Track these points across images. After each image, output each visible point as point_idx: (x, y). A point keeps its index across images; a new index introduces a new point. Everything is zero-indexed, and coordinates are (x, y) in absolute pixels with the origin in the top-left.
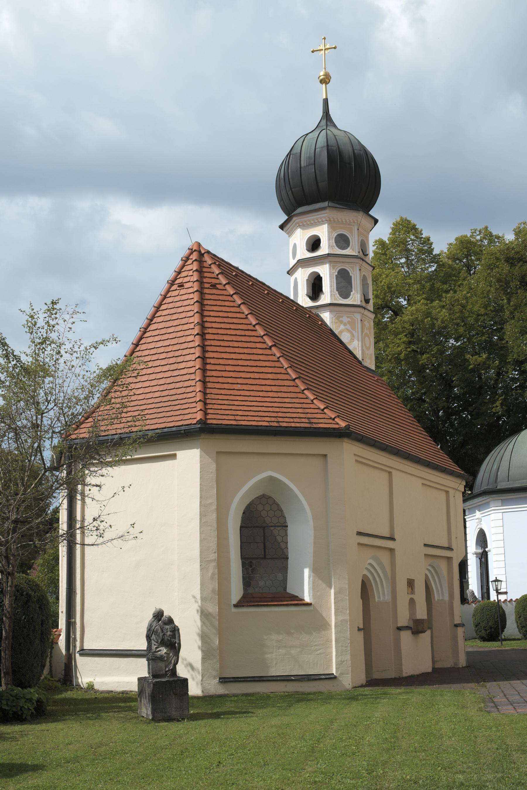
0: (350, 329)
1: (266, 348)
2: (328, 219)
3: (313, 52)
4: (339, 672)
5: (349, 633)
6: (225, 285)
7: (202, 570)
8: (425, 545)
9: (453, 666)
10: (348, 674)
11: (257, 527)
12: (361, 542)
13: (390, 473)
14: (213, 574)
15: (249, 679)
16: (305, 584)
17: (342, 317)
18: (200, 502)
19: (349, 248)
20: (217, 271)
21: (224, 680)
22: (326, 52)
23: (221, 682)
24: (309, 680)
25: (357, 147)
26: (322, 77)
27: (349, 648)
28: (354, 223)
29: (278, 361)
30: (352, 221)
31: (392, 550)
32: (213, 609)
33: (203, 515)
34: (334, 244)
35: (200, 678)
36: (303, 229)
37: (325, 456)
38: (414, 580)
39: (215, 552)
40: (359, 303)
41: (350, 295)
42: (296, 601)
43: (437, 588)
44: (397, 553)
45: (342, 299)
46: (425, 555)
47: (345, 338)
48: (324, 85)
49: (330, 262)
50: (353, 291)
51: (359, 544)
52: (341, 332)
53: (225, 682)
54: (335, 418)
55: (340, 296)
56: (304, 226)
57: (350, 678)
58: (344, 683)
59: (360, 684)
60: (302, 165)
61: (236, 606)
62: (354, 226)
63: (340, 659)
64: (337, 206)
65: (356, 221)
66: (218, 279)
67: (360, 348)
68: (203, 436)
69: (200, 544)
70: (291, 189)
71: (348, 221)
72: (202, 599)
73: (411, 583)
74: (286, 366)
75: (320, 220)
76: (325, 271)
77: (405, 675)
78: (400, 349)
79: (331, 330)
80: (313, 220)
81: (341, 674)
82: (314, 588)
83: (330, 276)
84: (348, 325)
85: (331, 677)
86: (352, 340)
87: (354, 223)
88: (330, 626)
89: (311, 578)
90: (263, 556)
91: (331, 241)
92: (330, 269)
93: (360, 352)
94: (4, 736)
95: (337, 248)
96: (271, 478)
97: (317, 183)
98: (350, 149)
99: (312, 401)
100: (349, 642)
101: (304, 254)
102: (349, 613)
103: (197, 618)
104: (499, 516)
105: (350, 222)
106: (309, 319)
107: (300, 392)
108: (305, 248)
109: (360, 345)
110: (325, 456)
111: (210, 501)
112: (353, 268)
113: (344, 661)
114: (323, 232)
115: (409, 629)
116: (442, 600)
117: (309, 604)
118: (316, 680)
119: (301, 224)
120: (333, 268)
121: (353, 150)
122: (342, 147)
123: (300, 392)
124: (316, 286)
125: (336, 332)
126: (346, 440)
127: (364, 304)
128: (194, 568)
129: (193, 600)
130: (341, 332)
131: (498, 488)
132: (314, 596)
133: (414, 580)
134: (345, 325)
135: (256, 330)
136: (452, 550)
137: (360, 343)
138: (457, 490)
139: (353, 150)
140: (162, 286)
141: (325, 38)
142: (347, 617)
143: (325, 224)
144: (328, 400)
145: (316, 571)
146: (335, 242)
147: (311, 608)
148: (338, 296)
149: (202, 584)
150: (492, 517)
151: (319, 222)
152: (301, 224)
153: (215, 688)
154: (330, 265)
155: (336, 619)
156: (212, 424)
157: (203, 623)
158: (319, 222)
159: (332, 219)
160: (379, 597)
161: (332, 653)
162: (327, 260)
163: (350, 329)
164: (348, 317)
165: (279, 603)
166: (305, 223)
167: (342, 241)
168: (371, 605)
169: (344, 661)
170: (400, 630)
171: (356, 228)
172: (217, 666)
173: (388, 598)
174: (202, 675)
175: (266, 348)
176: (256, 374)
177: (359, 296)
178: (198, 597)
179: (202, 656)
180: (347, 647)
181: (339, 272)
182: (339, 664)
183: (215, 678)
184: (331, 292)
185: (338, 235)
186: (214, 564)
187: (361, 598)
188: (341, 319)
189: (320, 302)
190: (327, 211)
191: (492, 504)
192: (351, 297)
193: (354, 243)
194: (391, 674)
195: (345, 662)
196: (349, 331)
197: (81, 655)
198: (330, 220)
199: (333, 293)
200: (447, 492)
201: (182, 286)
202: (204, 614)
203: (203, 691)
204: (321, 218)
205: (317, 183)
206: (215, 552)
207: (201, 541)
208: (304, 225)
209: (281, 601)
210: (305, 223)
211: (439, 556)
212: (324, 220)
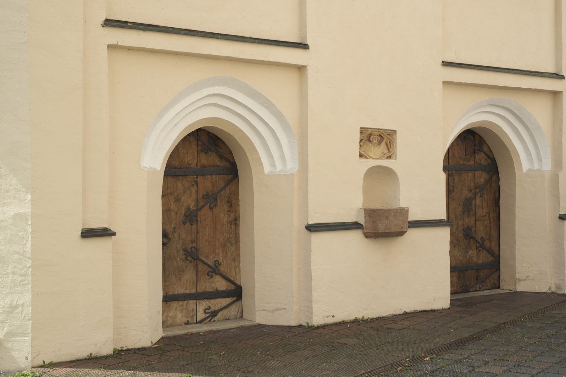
5: (29, 244)
8: (446, 64)
10: (25, 335)
12: (114, 42)
27: (29, 278)
31: (301, 69)
43: (526, 148)
44: (310, 73)
46: (444, 82)
51: (110, 47)
57: (29, 343)
58: (15, 354)
59: (83, 353)
94: (235, 298)
100: (29, 264)
102: (32, 200)
113: (16, 307)
115: (356, 228)
116: (538, 170)
133: (395, 131)
142: (27, 209)
160: (273, 165)
168: (254, 181)
169: (16, 307)
170: (310, 231)
173: (292, 166)
180: (24, 275)
187: (445, 169)
195: (20, 309)
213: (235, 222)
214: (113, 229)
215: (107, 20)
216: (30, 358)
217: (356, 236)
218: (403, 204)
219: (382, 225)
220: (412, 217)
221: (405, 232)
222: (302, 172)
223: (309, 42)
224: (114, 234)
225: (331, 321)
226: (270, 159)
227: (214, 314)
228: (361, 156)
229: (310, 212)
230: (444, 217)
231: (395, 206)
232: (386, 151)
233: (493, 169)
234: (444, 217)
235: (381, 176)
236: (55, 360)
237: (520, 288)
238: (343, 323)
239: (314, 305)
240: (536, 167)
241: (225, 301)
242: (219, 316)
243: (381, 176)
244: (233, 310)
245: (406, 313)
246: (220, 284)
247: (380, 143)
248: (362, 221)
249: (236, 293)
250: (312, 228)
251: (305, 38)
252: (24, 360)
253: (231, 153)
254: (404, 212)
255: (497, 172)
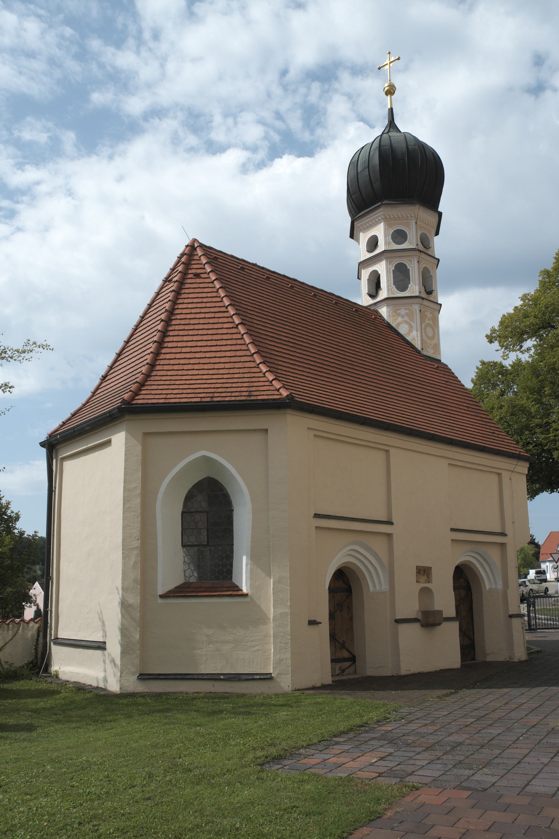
0: (409, 321)
1: (233, 328)
2: (383, 217)
4: (277, 672)
5: (289, 627)
7: (124, 558)
8: (453, 530)
9: (507, 660)
11: (200, 512)
13: (387, 451)
14: (135, 563)
15: (171, 677)
16: (244, 574)
17: (400, 309)
18: (124, 487)
19: (406, 243)
20: (204, 260)
21: (143, 677)
22: (391, 64)
23: (140, 679)
24: (240, 680)
25: (411, 143)
26: (386, 89)
27: (289, 645)
28: (411, 217)
29: (242, 338)
30: (409, 216)
31: (389, 536)
32: (134, 600)
33: (126, 500)
34: (391, 241)
35: (119, 674)
36: (364, 233)
37: (266, 430)
38: (417, 567)
39: (138, 539)
40: (417, 294)
41: (407, 288)
42: (234, 591)
44: (395, 537)
45: (399, 292)
46: (452, 540)
47: (403, 330)
49: (387, 258)
50: (411, 283)
51: (316, 527)
52: (399, 324)
53: (144, 679)
54: (280, 388)
55: (398, 289)
57: (290, 678)
58: (282, 685)
59: (310, 685)
60: (359, 171)
61: (161, 596)
62: (411, 220)
63: (278, 657)
64: (392, 202)
65: (413, 215)
66: (204, 269)
67: (419, 338)
68: (127, 417)
69: (123, 531)
71: (405, 216)
72: (123, 589)
73: (424, 572)
74: (248, 341)
76: (382, 268)
77: (403, 672)
78: (554, 360)
79: (388, 323)
80: (371, 221)
81: (279, 674)
82: (252, 576)
83: (387, 272)
84: (406, 317)
85: (268, 678)
86: (410, 331)
87: (411, 217)
88: (269, 619)
89: (249, 566)
90: (206, 543)
91: (387, 238)
92: (387, 265)
93: (419, 342)
95: (394, 244)
96: (206, 458)
97: (372, 185)
98: (404, 146)
99: (264, 374)
101: (365, 256)
102: (290, 605)
103: (119, 610)
105: (407, 217)
106: (369, 315)
107: (255, 367)
108: (366, 249)
109: (419, 335)
110: (266, 430)
111: (134, 485)
112: (410, 261)
113: (282, 660)
114: (379, 231)
117: (246, 595)
118: (248, 680)
119: (362, 228)
120: (390, 264)
121: (407, 146)
122: (394, 145)
123: (255, 367)
124: (375, 283)
125: (394, 325)
126: (289, 411)
127: (424, 295)
128: (118, 556)
129: (116, 591)
130: (399, 324)
132: (252, 586)
133: (431, 568)
134: (403, 317)
135: (228, 312)
136: (506, 535)
137: (419, 333)
138: (513, 471)
139: (407, 146)
140: (159, 283)
141: (389, 53)
142: (288, 610)
143: (381, 222)
144: (341, 385)
145: (254, 558)
146: (392, 239)
147: (248, 599)
148: (395, 289)
149: (124, 573)
152: (362, 228)
153: (134, 685)
154: (387, 261)
155: (274, 612)
156: (136, 404)
157: (123, 616)
159: (388, 217)
160: (375, 586)
161: (270, 650)
162: (383, 257)
163: (409, 321)
164: (406, 309)
165: (222, 593)
166: (365, 226)
167: (399, 236)
169: (282, 660)
170: (398, 623)
171: (414, 221)
172: (137, 661)
173: (385, 587)
174: (121, 671)
175: (233, 328)
176: (213, 353)
177: (417, 287)
178: (120, 588)
179: (121, 650)
180: (287, 643)
181: (395, 267)
182: (278, 663)
183: (134, 674)
184: (388, 286)
185: (395, 231)
186: (136, 552)
188: (398, 312)
189: (379, 299)
190: (381, 209)
192: (409, 289)
193: (411, 237)
194: (387, 672)
195: (284, 661)
196: (407, 323)
197: (55, 643)
198: (386, 218)
199: (390, 288)
200: (499, 475)
202: (124, 605)
203: (121, 688)
204: (377, 217)
205: (372, 185)
206: (138, 539)
207: (124, 527)
209: (216, 591)
211: (462, 541)
213: (351, 619)
214: (318, 620)
215: (315, 514)
216: (290, 686)
217: (417, 626)
218: (437, 607)
219: (429, 620)
220: (445, 615)
221: (439, 624)
222: (392, 591)
223: (394, 521)
224: (321, 623)
225: (408, 673)
226: (375, 583)
227: (343, 671)
228: (417, 581)
229: (397, 613)
230: (454, 616)
231: (432, 610)
232: (427, 579)
233: (349, 590)
234: (454, 616)
235: (426, 593)
236: (300, 688)
237: (489, 659)
238: (413, 675)
239: (401, 664)
240: (494, 587)
241: (347, 664)
242: (346, 672)
243: (426, 593)
244: (352, 669)
245: (441, 670)
246: (346, 654)
247: (424, 574)
248: (420, 617)
249: (353, 659)
250: (398, 621)
251: (392, 519)
252: (287, 687)
253: (349, 580)
254: (440, 612)
255: (351, 593)
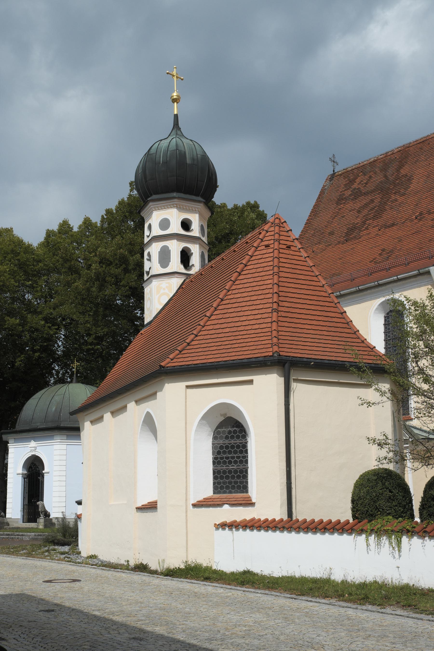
3: (168, 73)
6: (305, 258)
48: (175, 103)
56: (181, 209)
70: (197, 181)
75: (194, 209)
104: (64, 447)
119: (178, 206)
131: (62, 425)
150: (56, 447)
151: (192, 210)
152: (178, 206)
158: (192, 210)
166: (181, 207)
190: (176, 200)
191: (55, 437)
201: (269, 246)
204: (195, 207)
208: (180, 208)
210: (181, 207)
212: (197, 210)
